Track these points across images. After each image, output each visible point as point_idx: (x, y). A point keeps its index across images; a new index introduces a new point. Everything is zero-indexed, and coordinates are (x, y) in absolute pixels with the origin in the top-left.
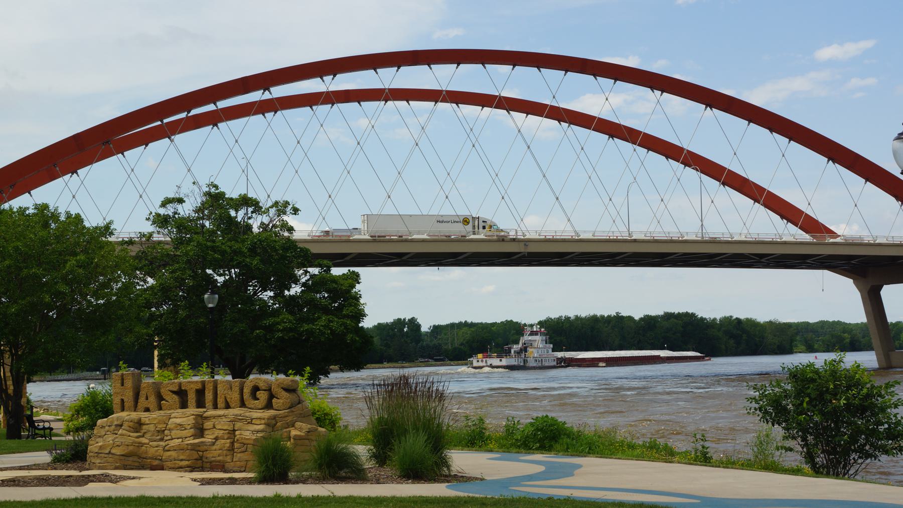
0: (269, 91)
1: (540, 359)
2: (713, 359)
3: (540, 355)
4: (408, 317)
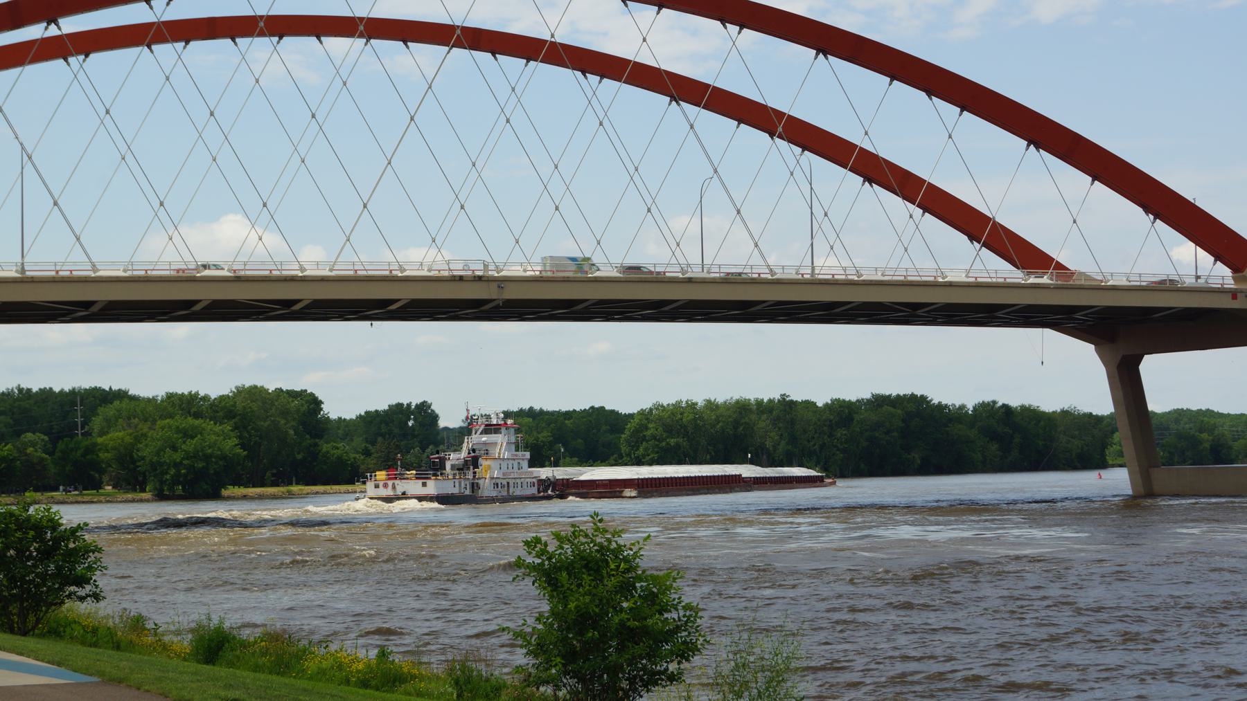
0: (57, 25)
1: (505, 482)
2: (841, 483)
4: (415, 401)
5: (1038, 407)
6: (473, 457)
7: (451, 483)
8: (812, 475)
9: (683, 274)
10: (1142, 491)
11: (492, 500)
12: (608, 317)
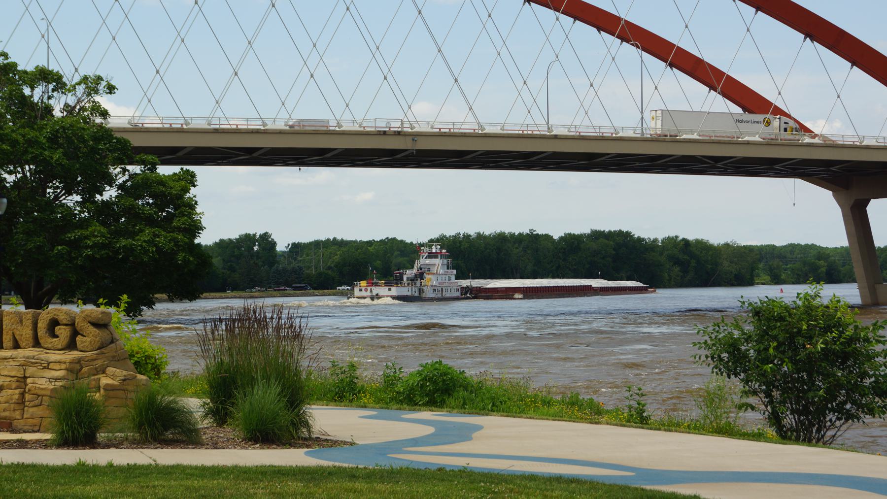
1: (440, 289)
2: (658, 291)
3: (439, 284)
4: (259, 232)
5: (708, 241)
6: (420, 273)
7: (406, 289)
8: (640, 286)
9: (412, 129)
10: (869, 301)
11: (432, 300)
12: (419, 164)
